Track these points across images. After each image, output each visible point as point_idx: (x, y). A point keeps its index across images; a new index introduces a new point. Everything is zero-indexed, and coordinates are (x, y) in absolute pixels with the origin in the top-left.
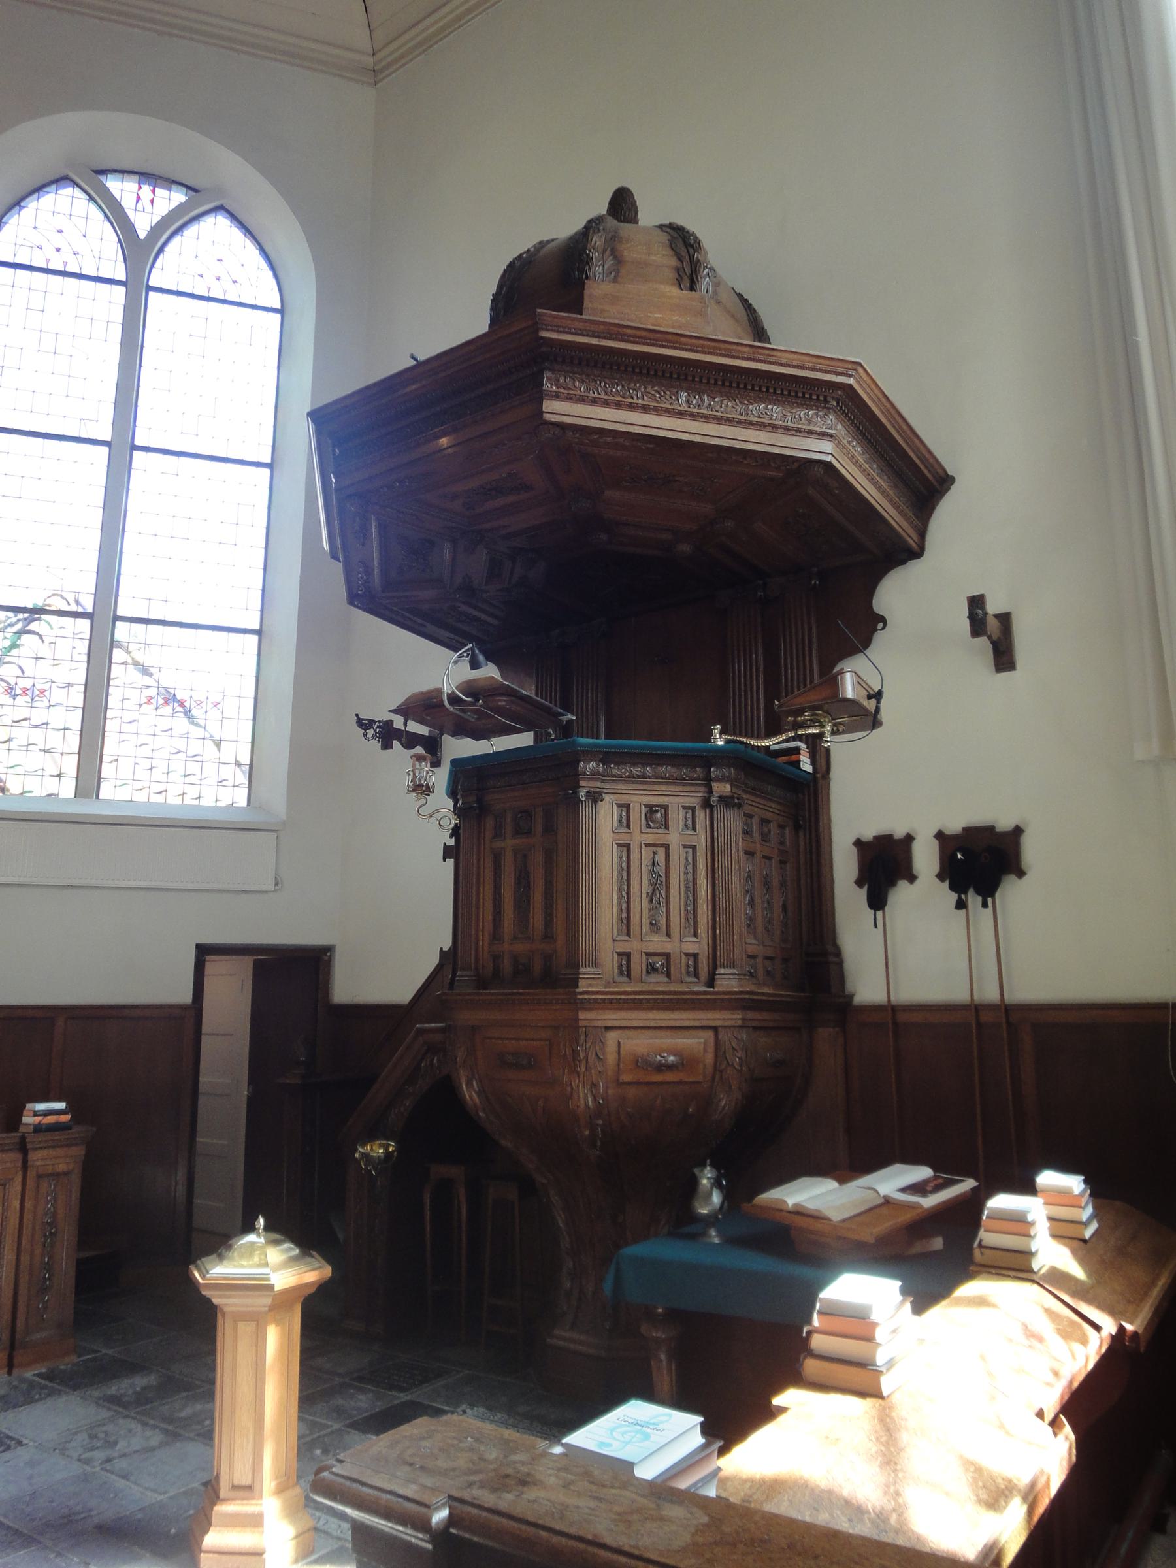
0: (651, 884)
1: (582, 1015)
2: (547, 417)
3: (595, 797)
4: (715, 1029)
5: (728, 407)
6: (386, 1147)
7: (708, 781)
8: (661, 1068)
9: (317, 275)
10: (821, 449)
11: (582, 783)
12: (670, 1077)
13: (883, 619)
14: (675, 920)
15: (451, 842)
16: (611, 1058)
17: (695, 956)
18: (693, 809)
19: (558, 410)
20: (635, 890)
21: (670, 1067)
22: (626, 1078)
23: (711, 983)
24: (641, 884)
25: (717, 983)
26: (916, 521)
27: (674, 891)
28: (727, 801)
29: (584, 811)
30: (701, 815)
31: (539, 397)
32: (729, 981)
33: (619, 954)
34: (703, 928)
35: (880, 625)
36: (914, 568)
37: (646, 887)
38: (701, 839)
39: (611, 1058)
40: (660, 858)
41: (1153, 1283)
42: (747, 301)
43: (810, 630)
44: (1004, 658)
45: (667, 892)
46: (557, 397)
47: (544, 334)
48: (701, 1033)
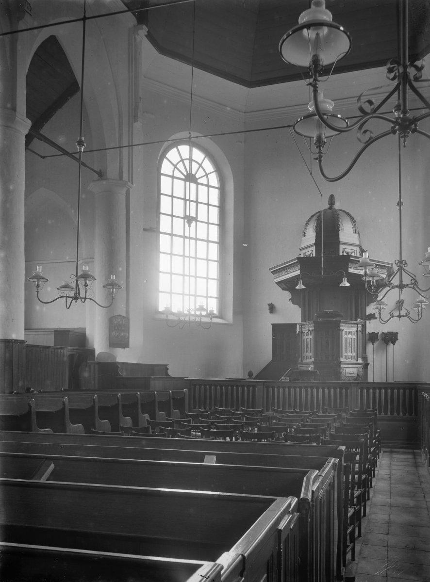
3: (343, 330)
19: (351, 270)
22: (346, 375)
23: (357, 360)
31: (348, 268)
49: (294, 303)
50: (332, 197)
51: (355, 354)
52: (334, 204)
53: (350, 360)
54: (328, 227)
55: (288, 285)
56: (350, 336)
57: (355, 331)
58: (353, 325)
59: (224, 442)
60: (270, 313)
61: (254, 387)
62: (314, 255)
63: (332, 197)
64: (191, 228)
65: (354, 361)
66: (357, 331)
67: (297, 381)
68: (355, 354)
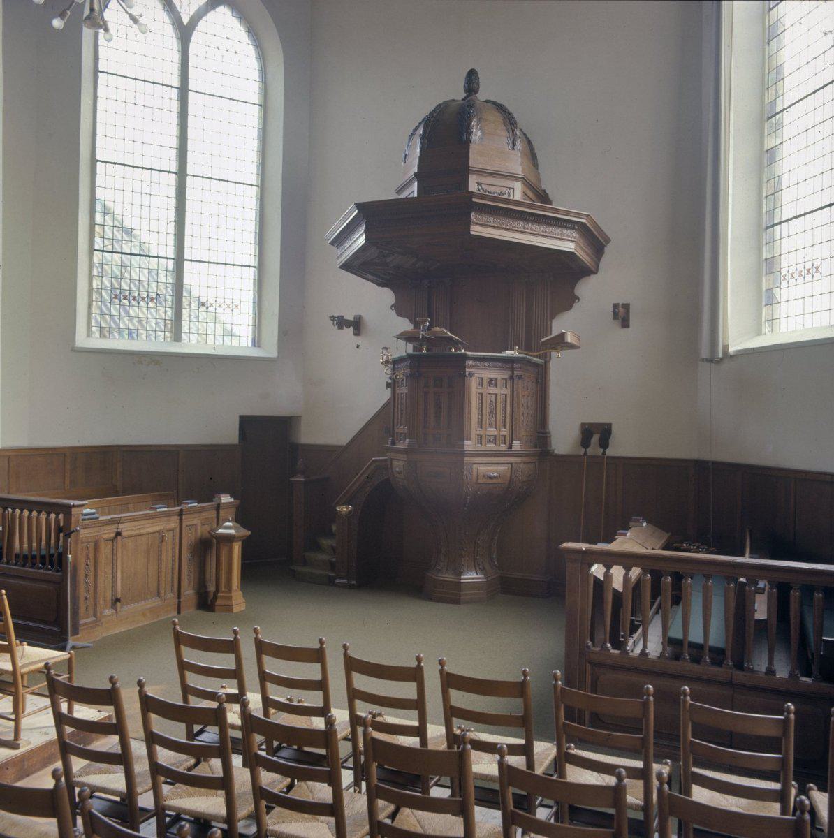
0: (490, 409)
1: (466, 458)
2: (472, 233)
3: (471, 375)
4: (511, 464)
5: (539, 228)
6: (347, 508)
7: (513, 369)
8: (491, 478)
9: (285, 56)
10: (569, 247)
11: (467, 370)
12: (494, 481)
13: (578, 298)
14: (498, 423)
15: (390, 381)
16: (475, 473)
17: (505, 436)
18: (506, 380)
19: (476, 230)
20: (484, 411)
21: (495, 477)
22: (480, 481)
23: (510, 447)
24: (486, 410)
25: (513, 447)
26: (595, 259)
27: (498, 412)
28: (520, 377)
29: (467, 380)
30: (509, 382)
31: (468, 223)
32: (517, 445)
33: (478, 435)
34: (508, 425)
35: (577, 300)
36: (593, 277)
37: (488, 410)
38: (508, 392)
39: (475, 473)
40: (493, 399)
41: (723, 343)
42: (528, 138)
43: (547, 300)
44: (625, 323)
45: (496, 412)
46: (477, 224)
47: (474, 200)
48: (506, 465)
49: (399, 314)
50: (472, 75)
51: (505, 432)
52: (476, 91)
53: (491, 446)
54: (446, 136)
55: (356, 266)
56: (492, 390)
57: (506, 377)
58: (491, 364)
59: (68, 685)
60: (355, 334)
61: (678, 578)
62: (416, 195)
63: (472, 75)
64: (540, 168)
65: (503, 447)
66: (511, 378)
67: (68, 467)
68: (505, 432)
